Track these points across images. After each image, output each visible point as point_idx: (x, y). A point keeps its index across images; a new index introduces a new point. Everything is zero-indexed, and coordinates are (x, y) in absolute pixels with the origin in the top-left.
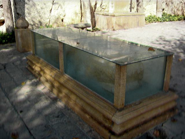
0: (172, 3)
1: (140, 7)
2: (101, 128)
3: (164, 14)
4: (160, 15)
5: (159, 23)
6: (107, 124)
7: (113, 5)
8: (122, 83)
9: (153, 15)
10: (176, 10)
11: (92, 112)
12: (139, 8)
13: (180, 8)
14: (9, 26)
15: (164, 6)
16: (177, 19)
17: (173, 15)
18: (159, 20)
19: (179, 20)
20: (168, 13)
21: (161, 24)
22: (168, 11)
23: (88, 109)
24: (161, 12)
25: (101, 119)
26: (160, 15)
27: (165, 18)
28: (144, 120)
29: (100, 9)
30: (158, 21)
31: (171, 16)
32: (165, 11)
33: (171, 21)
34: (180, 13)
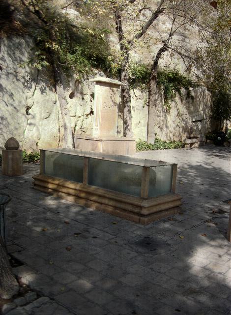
0: (167, 127)
1: (129, 131)
2: (132, 215)
3: (157, 140)
4: (152, 141)
5: (151, 151)
6: (136, 210)
7: (98, 127)
8: (147, 180)
9: (143, 141)
10: (171, 135)
11: (122, 206)
12: (127, 132)
13: (177, 134)
14: (16, 147)
15: (157, 130)
16: (173, 146)
17: (168, 142)
18: (151, 147)
19: (175, 147)
20: (162, 140)
21: (154, 151)
22: (162, 137)
23: (118, 205)
24: (153, 137)
25: (130, 208)
26: (152, 141)
27: (158, 145)
28: (160, 209)
29: (80, 132)
30: (150, 148)
31: (165, 142)
32: (159, 137)
33: (166, 149)
34: (176, 139)
